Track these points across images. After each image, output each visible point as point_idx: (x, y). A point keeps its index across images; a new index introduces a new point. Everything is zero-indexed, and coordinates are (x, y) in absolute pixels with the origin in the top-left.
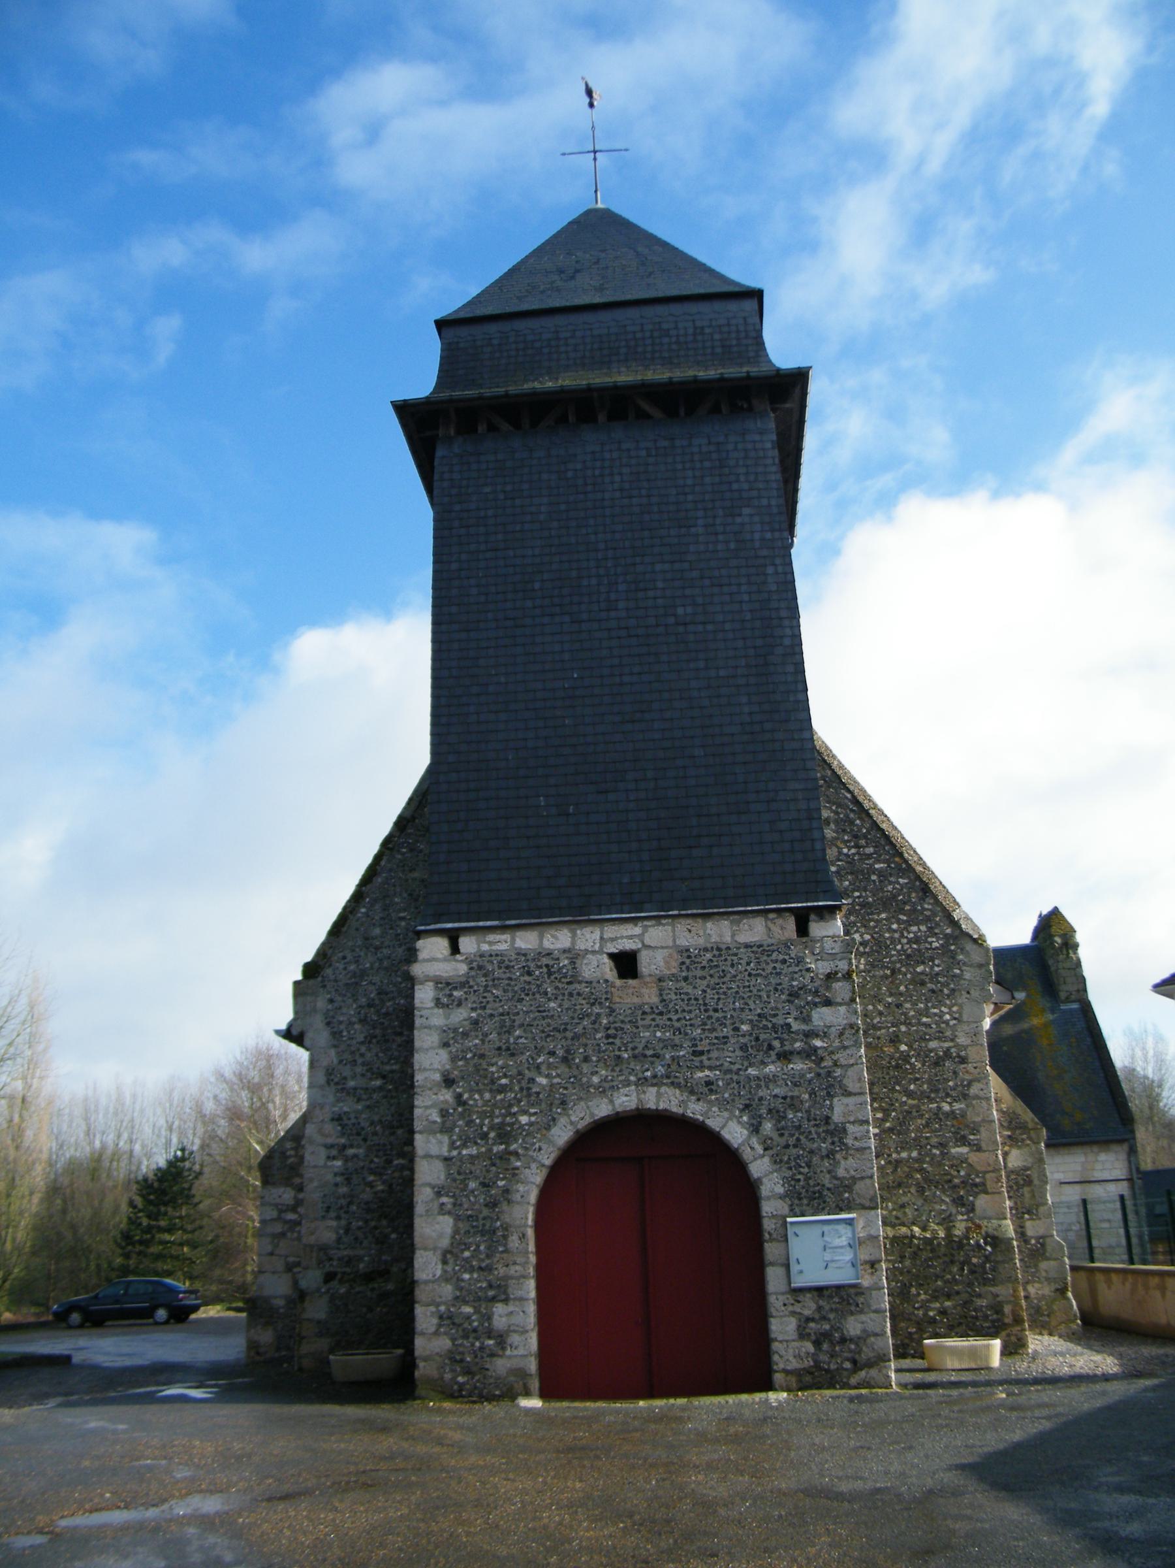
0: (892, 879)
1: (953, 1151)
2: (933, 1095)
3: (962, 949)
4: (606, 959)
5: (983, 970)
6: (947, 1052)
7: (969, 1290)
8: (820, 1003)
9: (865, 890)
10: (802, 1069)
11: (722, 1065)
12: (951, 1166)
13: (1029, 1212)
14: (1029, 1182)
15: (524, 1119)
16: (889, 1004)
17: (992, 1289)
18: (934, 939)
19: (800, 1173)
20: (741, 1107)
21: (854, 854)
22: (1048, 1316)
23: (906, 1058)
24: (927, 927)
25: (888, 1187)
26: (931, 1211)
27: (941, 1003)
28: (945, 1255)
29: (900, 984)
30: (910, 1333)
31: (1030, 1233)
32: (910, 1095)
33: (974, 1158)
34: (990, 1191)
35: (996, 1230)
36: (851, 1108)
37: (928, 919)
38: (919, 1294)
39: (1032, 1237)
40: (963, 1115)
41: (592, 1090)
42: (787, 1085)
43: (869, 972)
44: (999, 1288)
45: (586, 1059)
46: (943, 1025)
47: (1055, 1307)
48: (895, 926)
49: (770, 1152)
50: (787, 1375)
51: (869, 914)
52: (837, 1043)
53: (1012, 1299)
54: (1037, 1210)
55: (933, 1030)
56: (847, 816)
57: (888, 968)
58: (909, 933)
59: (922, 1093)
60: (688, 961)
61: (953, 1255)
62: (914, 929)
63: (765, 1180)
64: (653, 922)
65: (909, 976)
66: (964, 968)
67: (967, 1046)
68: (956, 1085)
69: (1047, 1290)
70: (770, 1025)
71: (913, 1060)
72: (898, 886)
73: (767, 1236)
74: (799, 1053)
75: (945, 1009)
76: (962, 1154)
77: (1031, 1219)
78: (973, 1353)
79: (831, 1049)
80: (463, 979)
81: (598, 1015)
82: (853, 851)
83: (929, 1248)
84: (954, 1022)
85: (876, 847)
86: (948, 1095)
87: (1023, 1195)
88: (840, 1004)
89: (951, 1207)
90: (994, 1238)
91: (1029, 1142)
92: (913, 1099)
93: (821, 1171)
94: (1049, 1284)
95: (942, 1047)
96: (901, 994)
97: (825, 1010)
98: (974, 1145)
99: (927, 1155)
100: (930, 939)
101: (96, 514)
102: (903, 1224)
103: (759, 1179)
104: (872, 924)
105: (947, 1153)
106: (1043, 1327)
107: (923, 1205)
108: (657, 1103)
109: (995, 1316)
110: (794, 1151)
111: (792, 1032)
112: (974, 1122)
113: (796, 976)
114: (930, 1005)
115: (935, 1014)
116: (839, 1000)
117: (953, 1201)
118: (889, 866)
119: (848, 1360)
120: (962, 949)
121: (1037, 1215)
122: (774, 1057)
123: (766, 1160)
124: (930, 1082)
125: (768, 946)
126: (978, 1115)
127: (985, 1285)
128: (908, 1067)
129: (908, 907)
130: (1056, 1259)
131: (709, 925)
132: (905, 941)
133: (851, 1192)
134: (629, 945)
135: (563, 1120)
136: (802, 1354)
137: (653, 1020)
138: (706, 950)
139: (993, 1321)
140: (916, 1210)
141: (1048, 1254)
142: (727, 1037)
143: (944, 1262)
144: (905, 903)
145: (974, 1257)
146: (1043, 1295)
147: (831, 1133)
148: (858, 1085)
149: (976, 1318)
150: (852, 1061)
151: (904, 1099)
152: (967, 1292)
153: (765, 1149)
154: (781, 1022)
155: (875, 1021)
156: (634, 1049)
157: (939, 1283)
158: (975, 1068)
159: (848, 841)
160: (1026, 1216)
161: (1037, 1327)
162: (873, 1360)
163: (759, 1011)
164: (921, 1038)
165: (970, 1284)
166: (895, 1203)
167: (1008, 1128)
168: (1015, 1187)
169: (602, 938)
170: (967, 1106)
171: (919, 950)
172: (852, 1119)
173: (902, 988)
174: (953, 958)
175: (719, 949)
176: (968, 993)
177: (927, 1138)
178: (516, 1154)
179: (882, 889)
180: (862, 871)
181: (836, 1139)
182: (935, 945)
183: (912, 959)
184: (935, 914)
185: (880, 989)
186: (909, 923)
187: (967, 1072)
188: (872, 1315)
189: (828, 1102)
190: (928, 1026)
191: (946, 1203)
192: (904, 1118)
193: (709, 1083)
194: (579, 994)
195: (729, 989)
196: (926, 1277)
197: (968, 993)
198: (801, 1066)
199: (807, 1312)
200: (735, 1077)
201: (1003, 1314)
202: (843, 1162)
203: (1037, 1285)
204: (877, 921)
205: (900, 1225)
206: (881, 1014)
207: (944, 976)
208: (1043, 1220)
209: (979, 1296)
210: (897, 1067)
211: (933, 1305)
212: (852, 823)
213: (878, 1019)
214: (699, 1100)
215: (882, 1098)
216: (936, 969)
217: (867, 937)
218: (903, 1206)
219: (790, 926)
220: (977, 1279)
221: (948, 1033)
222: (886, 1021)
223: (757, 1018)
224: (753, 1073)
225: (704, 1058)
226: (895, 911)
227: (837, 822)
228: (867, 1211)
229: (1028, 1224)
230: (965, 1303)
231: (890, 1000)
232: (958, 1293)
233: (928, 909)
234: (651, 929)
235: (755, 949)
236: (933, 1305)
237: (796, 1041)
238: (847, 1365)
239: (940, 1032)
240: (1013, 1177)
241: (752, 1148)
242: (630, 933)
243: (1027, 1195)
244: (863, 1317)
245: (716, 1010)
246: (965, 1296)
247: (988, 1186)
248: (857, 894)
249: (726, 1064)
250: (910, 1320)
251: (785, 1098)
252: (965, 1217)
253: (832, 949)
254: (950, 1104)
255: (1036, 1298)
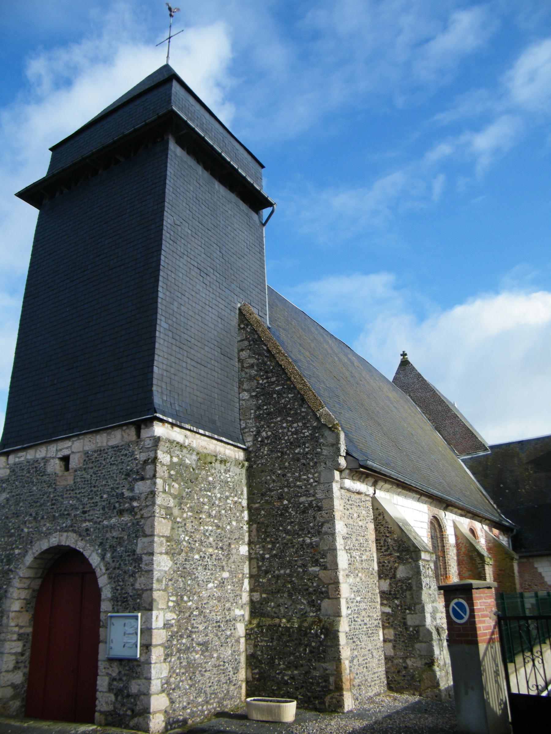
0: (285, 395)
1: (310, 569)
2: (300, 533)
3: (322, 436)
4: (57, 461)
5: (334, 448)
6: (310, 504)
7: (309, 664)
8: (138, 479)
9: (270, 404)
10: (127, 520)
11: (93, 519)
12: (309, 579)
13: (409, 609)
14: (410, 588)
15: (17, 551)
16: (279, 474)
17: (324, 665)
18: (306, 431)
19: (119, 585)
20: (99, 544)
21: (265, 383)
22: (419, 681)
23: (286, 508)
24: (303, 423)
25: (272, 592)
26: (295, 609)
27: (308, 472)
28: (296, 639)
29: (286, 461)
30: (273, 690)
31: (409, 623)
32: (288, 532)
33: (322, 574)
34: (331, 597)
35: (330, 624)
36: (146, 544)
37: (304, 418)
38: (279, 664)
39: (410, 626)
40: (317, 546)
41: (42, 535)
42: (119, 530)
43: (269, 455)
44: (328, 664)
45: (43, 518)
46: (309, 486)
47: (424, 676)
48: (285, 425)
49: (108, 572)
50: (101, 715)
51: (271, 419)
52: (143, 504)
53: (335, 673)
54: (414, 607)
55: (303, 490)
56: (263, 360)
57: (279, 451)
58: (292, 428)
59: (295, 531)
60: (87, 459)
61: (300, 639)
62: (295, 425)
63: (103, 589)
64: (76, 439)
65: (291, 456)
66: (323, 447)
67: (323, 499)
68: (314, 525)
69: (419, 663)
70: (115, 494)
71: (290, 510)
72: (287, 399)
73: (101, 624)
74: (127, 510)
75: (310, 476)
76: (315, 571)
77: (410, 613)
78: (269, 710)
79: (140, 507)
80: (7, 478)
81: (50, 492)
82: (265, 381)
83: (287, 634)
84: (316, 484)
85: (277, 376)
86: (309, 532)
87: (406, 597)
88: (148, 479)
89: (307, 607)
90: (327, 629)
91: (410, 560)
92: (289, 535)
93: (129, 585)
94: (421, 659)
95: (307, 501)
96: (286, 468)
97: (140, 483)
98: (323, 565)
99: (295, 571)
100: (303, 431)
101: (366, 273)
102: (278, 617)
103: (101, 588)
104: (272, 425)
105: (306, 571)
106: (416, 689)
107: (291, 605)
108: (66, 542)
109: (324, 684)
110: (117, 571)
111: (124, 498)
112: (323, 550)
113: (130, 463)
114: (302, 473)
115: (305, 480)
116: (148, 477)
117: (308, 603)
118: (283, 388)
119: (129, 709)
120: (322, 436)
121: (414, 611)
122: (115, 514)
123: (106, 576)
124: (299, 524)
125: (121, 446)
126: (327, 545)
127: (319, 661)
128: (287, 514)
129: (292, 412)
130: (425, 642)
131: (98, 437)
132: (290, 433)
133: (141, 599)
134: (66, 452)
135: (30, 552)
136: (109, 702)
137: (70, 494)
138: (95, 452)
139: (323, 687)
140: (286, 608)
141: (420, 638)
142: (97, 502)
143: (296, 644)
144: (291, 409)
145: (313, 641)
146: (417, 667)
147: (135, 560)
148: (151, 530)
149: (312, 683)
150: (149, 515)
151: (284, 535)
152: (307, 665)
153: (107, 570)
154: (120, 492)
155: (271, 486)
156: (61, 511)
157: (292, 658)
158: (327, 513)
159: (263, 376)
160: (407, 611)
161: (411, 689)
162: (141, 711)
163: (112, 486)
164: (296, 495)
165: (310, 660)
166: (275, 603)
167: (398, 551)
168: (401, 592)
169: (57, 450)
170: (320, 539)
171: (297, 439)
172: (145, 552)
173: (287, 464)
174: (317, 441)
175: (101, 451)
176: (325, 464)
177: (296, 561)
178: (11, 571)
179: (279, 402)
180: (269, 393)
181: (137, 564)
182: (307, 434)
183: (293, 444)
184: (307, 414)
185: (274, 465)
186: (292, 422)
187: (322, 516)
188: (144, 681)
189: (135, 541)
190: (300, 487)
191: (304, 604)
192: (284, 547)
193: (87, 530)
194: (45, 482)
195: (102, 473)
196: (284, 654)
197: (325, 464)
198: (127, 518)
199: (114, 675)
200: (98, 526)
201: (329, 683)
202: (138, 579)
203: (412, 659)
204: (276, 423)
205: (276, 618)
206: (274, 481)
207: (311, 454)
208: (418, 614)
209: (315, 669)
210: (282, 515)
211: (286, 673)
212: (265, 364)
213: (272, 485)
214: (82, 540)
215: (272, 535)
216: (307, 450)
217: (269, 433)
218: (279, 606)
219: (132, 431)
220: (314, 657)
221: (312, 492)
222: (277, 486)
223: (110, 490)
224: (106, 523)
225: (87, 515)
226: (285, 416)
227: (257, 365)
228: (147, 612)
229: (409, 617)
230: (306, 673)
231: (279, 472)
232: (302, 665)
233: (304, 412)
234: (75, 442)
235: (115, 449)
236: (286, 673)
237: (126, 503)
238: (129, 712)
239: (307, 491)
240: (399, 584)
241: (101, 569)
242: (66, 446)
243: (408, 597)
244: (139, 681)
245: (94, 487)
246: (306, 668)
247: (330, 594)
248: (265, 407)
249: (95, 518)
250: (273, 680)
251: (117, 538)
252: (315, 614)
253: (149, 444)
254: (310, 538)
255: (412, 669)
